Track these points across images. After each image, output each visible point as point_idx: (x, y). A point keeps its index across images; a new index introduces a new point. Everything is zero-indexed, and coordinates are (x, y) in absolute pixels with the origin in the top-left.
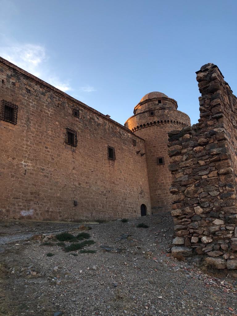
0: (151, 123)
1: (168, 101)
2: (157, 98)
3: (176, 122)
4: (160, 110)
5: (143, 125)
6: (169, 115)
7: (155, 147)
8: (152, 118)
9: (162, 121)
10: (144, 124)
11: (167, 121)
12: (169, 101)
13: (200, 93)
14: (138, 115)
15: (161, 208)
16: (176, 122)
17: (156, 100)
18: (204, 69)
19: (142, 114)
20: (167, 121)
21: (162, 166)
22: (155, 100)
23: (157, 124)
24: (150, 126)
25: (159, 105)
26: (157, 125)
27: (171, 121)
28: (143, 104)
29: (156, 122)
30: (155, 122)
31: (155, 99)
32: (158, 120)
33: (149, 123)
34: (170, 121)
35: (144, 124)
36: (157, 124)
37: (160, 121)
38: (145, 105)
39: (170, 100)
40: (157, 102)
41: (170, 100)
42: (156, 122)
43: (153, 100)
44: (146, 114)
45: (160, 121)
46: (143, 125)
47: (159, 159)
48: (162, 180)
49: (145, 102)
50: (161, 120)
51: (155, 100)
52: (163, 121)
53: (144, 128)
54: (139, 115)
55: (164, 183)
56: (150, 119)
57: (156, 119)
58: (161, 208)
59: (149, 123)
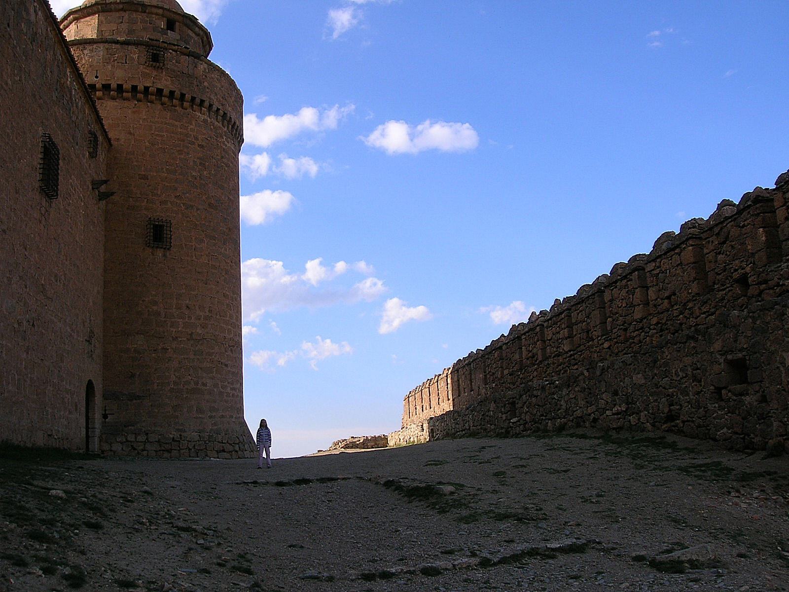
0: (147, 89)
1: (195, 33)
2: (169, 10)
3: (221, 112)
4: (185, 54)
5: (114, 86)
6: (206, 84)
7: (145, 177)
8: (155, 73)
9: (183, 95)
10: (120, 87)
11: (198, 101)
12: (198, 35)
13: (746, 197)
14: (101, 45)
15: (139, 397)
16: (221, 112)
17: (163, 16)
18: (263, 420)
19: (118, 46)
20: (198, 101)
21: (160, 253)
22: (157, 14)
23: (165, 99)
24: (139, 101)
25: (167, 34)
26: (162, 104)
27: (211, 106)
28: (111, 11)
29: (166, 92)
30: (160, 92)
31: (160, 11)
32: (172, 88)
33: (141, 87)
34: (207, 104)
35: (120, 87)
36: (165, 99)
37: (177, 94)
38: (117, 14)
39: (201, 33)
40: (163, 25)
41: (201, 33)
42: (166, 92)
43: (155, 10)
44: (135, 54)
45: (177, 94)
46: (114, 86)
47: (155, 226)
48: (155, 303)
49: (121, 6)
50: (184, 92)
51: (157, 14)
52: (188, 97)
53: (113, 98)
54: (107, 45)
55: (159, 314)
56: (145, 75)
57: (165, 83)
58: (139, 397)
59: (141, 87)
